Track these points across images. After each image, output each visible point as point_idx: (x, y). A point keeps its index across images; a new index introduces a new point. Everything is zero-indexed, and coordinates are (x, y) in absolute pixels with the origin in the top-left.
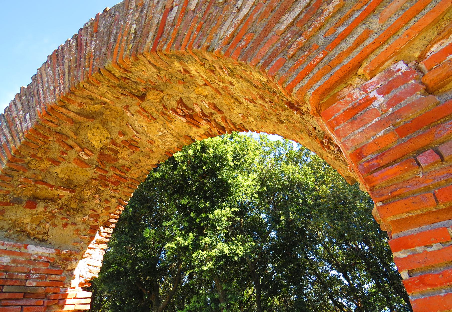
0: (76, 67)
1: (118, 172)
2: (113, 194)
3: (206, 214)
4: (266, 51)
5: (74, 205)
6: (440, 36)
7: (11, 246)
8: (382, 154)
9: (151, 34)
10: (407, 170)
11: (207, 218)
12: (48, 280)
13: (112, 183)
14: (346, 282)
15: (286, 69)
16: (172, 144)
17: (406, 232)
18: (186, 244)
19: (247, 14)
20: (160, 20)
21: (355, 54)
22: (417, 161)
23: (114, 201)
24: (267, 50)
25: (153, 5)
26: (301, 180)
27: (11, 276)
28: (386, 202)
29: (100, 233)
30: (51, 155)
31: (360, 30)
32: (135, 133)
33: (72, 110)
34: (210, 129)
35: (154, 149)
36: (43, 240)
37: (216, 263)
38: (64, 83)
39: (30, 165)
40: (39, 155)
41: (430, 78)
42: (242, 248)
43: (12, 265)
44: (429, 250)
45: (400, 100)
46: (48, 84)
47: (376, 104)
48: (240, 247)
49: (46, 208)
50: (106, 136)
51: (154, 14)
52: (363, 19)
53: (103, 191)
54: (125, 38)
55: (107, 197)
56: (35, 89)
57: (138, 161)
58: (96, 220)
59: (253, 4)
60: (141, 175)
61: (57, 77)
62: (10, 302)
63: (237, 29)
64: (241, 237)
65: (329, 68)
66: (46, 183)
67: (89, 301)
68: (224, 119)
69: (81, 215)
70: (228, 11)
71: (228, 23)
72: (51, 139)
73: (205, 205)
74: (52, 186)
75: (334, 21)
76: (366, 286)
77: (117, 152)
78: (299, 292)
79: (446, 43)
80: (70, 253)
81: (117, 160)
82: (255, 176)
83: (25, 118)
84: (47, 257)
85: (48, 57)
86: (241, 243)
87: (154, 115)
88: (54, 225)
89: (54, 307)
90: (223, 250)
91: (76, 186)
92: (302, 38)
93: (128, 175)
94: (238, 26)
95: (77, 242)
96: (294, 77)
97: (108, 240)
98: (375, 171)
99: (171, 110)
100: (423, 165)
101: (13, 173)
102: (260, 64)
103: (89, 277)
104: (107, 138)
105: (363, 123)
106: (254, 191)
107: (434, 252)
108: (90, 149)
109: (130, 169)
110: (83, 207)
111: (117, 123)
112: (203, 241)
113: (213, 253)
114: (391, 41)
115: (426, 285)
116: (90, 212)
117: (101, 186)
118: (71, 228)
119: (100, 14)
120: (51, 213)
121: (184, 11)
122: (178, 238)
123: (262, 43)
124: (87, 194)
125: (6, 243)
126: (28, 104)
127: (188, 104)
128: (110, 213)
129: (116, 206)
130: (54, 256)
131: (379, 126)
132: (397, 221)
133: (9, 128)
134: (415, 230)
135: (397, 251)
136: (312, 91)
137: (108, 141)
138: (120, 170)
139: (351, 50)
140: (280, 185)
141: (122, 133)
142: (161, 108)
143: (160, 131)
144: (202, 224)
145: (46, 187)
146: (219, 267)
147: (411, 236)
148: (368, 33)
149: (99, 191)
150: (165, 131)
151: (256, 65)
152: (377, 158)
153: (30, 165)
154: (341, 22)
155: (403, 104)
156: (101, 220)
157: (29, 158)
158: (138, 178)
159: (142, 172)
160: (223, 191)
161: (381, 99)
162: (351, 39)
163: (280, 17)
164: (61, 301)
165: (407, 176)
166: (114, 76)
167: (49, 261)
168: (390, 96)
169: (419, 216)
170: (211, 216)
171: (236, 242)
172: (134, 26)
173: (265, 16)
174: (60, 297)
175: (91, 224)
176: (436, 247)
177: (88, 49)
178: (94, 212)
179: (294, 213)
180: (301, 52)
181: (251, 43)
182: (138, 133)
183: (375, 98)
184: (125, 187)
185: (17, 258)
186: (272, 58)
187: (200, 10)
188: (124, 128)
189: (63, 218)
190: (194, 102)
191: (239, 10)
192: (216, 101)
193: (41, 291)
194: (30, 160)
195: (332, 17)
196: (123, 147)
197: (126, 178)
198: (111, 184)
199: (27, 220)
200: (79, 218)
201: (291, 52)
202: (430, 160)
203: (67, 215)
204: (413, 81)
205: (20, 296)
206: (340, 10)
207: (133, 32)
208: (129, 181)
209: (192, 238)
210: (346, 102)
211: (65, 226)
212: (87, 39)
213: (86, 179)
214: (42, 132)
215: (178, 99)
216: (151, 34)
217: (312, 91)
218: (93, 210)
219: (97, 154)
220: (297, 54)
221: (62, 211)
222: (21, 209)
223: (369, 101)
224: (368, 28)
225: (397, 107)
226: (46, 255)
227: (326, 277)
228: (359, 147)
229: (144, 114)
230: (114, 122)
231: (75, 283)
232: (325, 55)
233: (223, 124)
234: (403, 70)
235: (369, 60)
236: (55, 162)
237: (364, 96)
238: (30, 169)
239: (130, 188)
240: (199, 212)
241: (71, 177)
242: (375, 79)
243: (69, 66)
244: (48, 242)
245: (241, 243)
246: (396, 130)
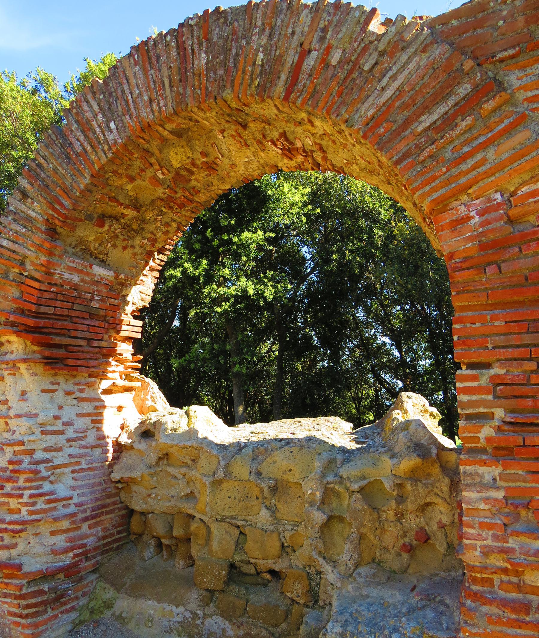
0: (180, 81)
1: (187, 194)
2: (174, 217)
3: (229, 236)
4: (402, 148)
5: (135, 227)
6: (533, 179)
8: (465, 259)
9: (283, 77)
10: (477, 275)
11: (230, 242)
12: (108, 304)
13: (178, 205)
14: (396, 353)
15: (415, 173)
16: (254, 171)
17: (464, 314)
18: (197, 274)
19: (391, 97)
20: (295, 61)
21: (469, 176)
22: (485, 269)
23: (174, 225)
24: (402, 147)
25: (285, 35)
26: (371, 205)
27: (80, 294)
28: (458, 293)
29: (154, 259)
30: (131, 172)
31: (479, 157)
32: (220, 156)
33: (168, 128)
34: (303, 163)
35: (232, 174)
36: (103, 261)
37: (233, 305)
38: (165, 98)
39: (109, 181)
40: (120, 171)
41: (513, 212)
42: (273, 291)
44: (473, 326)
45: (490, 223)
46: (139, 90)
47: (473, 222)
48: (270, 288)
49: (110, 226)
50: (188, 155)
51: (287, 48)
52: (484, 146)
53: (165, 214)
54: (250, 68)
55: (168, 220)
56: (119, 90)
57: (210, 184)
58: (153, 245)
59: (398, 89)
60: (208, 199)
61: (152, 86)
62: (80, 321)
63: (379, 110)
64: (272, 275)
65: (449, 181)
66: (117, 201)
67: (140, 330)
68: (325, 158)
69: (140, 238)
70: (372, 85)
71: (370, 100)
72: (136, 156)
73: (229, 222)
74: (121, 204)
75: (463, 139)
76: (422, 363)
77: (192, 173)
78: (335, 357)
79: (534, 187)
80: (126, 279)
81: (190, 180)
82: (308, 190)
83: (108, 127)
85: (132, 48)
86: (272, 283)
87: (249, 142)
88: (115, 246)
89: (111, 331)
90: (245, 289)
91: (141, 205)
92: (434, 147)
93: (196, 198)
94: (381, 108)
95: (133, 267)
96: (419, 182)
97: (161, 268)
98: (458, 271)
99: (271, 141)
100: (488, 274)
101: (94, 189)
102: (394, 159)
103: (140, 305)
104: (189, 157)
105: (460, 234)
106: (301, 211)
107: (476, 328)
108: (168, 167)
109: (199, 191)
110: (143, 229)
111: (202, 141)
112: (221, 273)
113: (232, 290)
114: (497, 175)
115: (465, 345)
116: (148, 235)
117: (164, 207)
118: (129, 251)
119: (210, 11)
120: (114, 232)
121: (324, 62)
122: (186, 265)
123: (399, 138)
124: (149, 215)
126: (109, 108)
127: (291, 138)
128: (168, 239)
129: (174, 230)
130: (112, 279)
131: (470, 239)
132: (461, 306)
133: (83, 131)
134: (470, 313)
135: (455, 324)
136: (430, 199)
137: (188, 161)
138: (190, 193)
139: (468, 172)
140: (340, 208)
141: (204, 154)
142: (259, 136)
143: (247, 157)
144: (221, 250)
145: (116, 204)
146: (238, 312)
147: (466, 317)
148: (484, 161)
149: (161, 213)
150: (253, 158)
151: (390, 159)
152: (461, 262)
153: (109, 181)
154: (467, 142)
155: (490, 227)
156: (157, 245)
157: (110, 174)
158: (205, 202)
159: (210, 196)
160: (257, 205)
161: (477, 219)
162: (471, 162)
163: (419, 116)
164: (118, 326)
165: (476, 278)
166: (229, 106)
168: (484, 218)
169: (475, 305)
170: (235, 239)
171: (266, 280)
172: (261, 55)
173: (406, 108)
174: (117, 322)
175: (148, 248)
176: (478, 325)
177: (196, 62)
178: (153, 236)
179: (351, 251)
180: (430, 159)
181: (389, 133)
182: (222, 156)
183: (473, 217)
184: (189, 210)
186: (405, 156)
187: (342, 68)
188: (209, 149)
189: (124, 240)
190: (298, 136)
191: (383, 89)
192: (323, 143)
193: (102, 313)
194: (111, 176)
195: (462, 134)
196: (201, 168)
197: (192, 201)
198: (176, 207)
199: (91, 239)
200: (138, 241)
201: (422, 158)
202: (493, 271)
203: (129, 236)
204: (502, 211)
205: (86, 315)
206: (470, 129)
207: (260, 63)
208: (194, 205)
209: (206, 267)
210: (452, 214)
211: (125, 248)
212: (192, 44)
213: (152, 198)
214: (130, 148)
215: (281, 131)
216: (283, 77)
217: (430, 199)
218: (152, 233)
219: (173, 174)
220: (427, 160)
221: (124, 233)
222: (91, 226)
223: (469, 218)
224: (485, 157)
225: (485, 228)
226: (107, 277)
227: (372, 344)
228: (452, 251)
229: (239, 139)
230: (199, 140)
231: (129, 309)
232: (448, 170)
233: (320, 160)
234: (499, 201)
235: (478, 185)
236: (132, 179)
237: (466, 213)
238: (108, 185)
239: (193, 212)
240: (219, 230)
241: (138, 195)
242: (478, 201)
243: (169, 76)
244: (107, 263)
245: (272, 283)
246: (480, 245)
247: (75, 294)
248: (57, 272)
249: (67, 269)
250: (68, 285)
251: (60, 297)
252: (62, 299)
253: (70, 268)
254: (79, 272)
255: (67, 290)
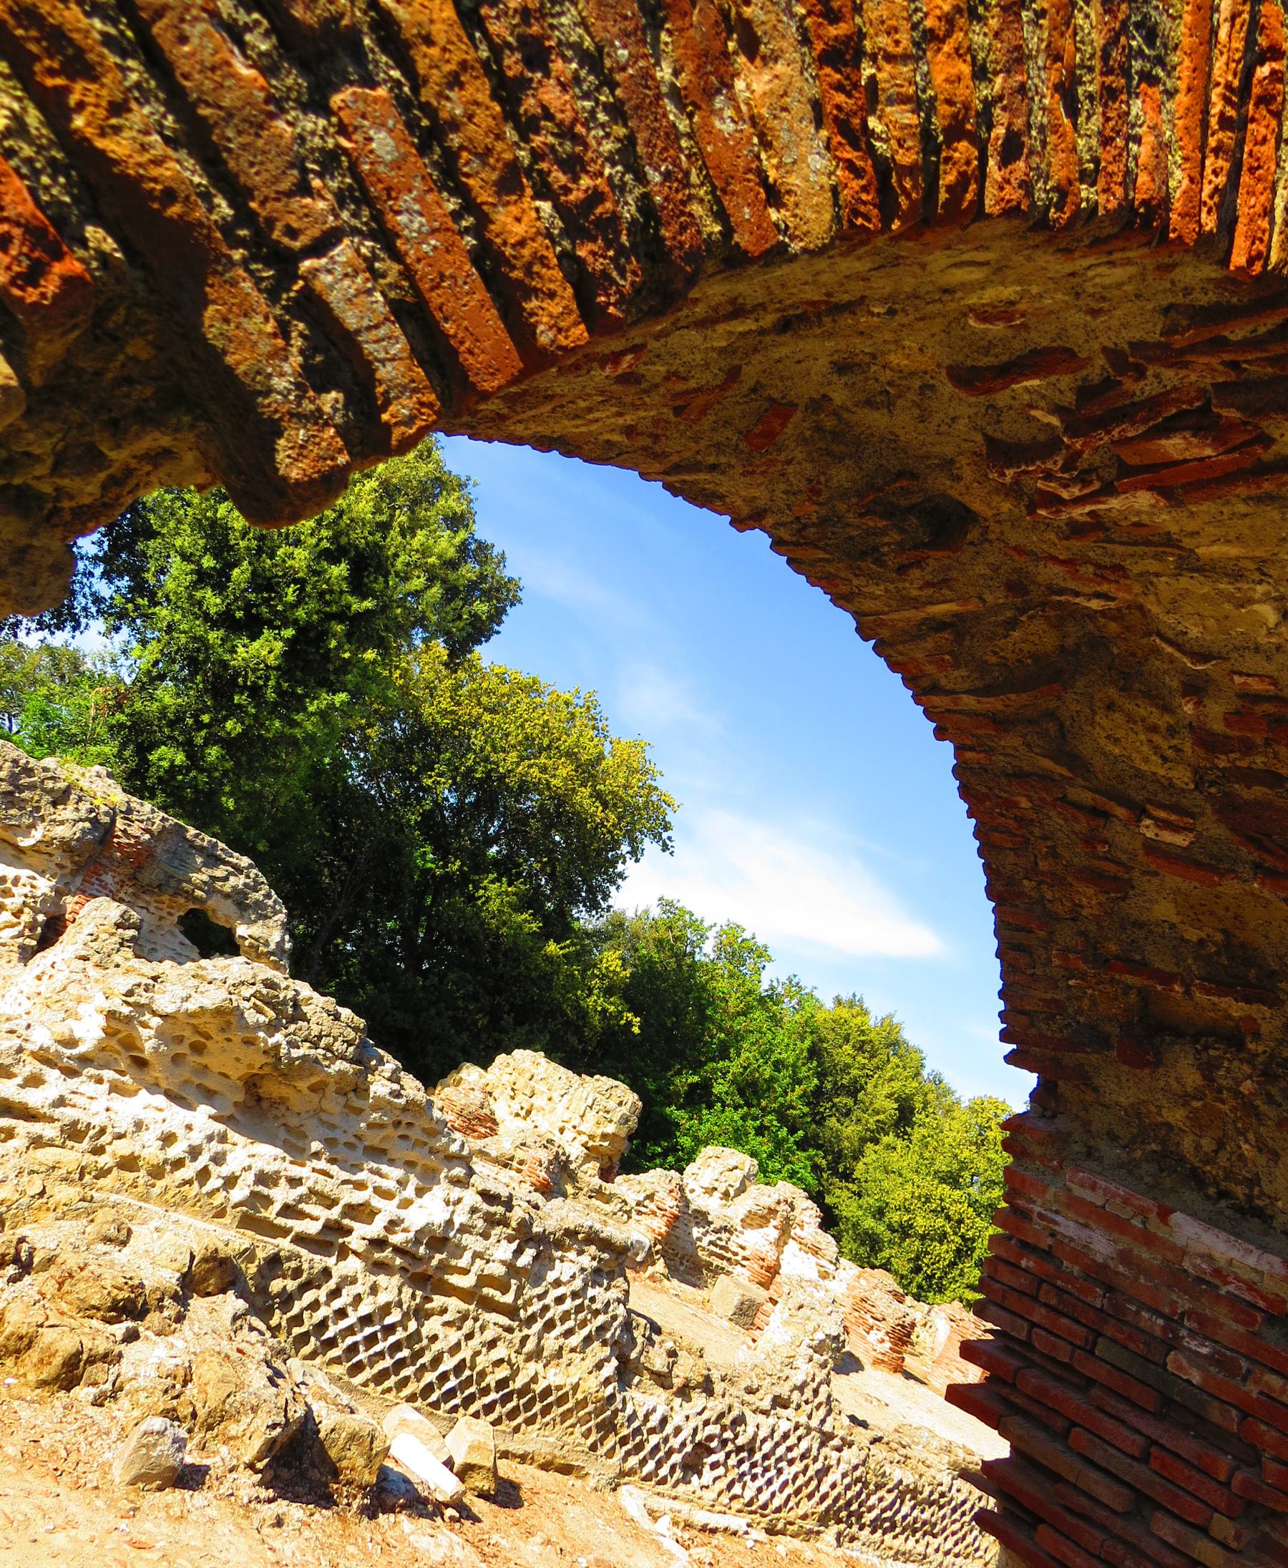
7: (1118, 1200)
43: (1121, 1268)
84: (1251, 1287)
125: (1103, 1184)
167: (1261, 1304)
185: (1136, 1252)
226: (1246, 1276)
247: (1098, 1300)
248: (1037, 1209)
249: (1069, 1206)
250: (1075, 1262)
251: (1046, 1294)
252: (1053, 1302)
253: (1075, 1204)
254: (1115, 1225)
255: (1070, 1278)
